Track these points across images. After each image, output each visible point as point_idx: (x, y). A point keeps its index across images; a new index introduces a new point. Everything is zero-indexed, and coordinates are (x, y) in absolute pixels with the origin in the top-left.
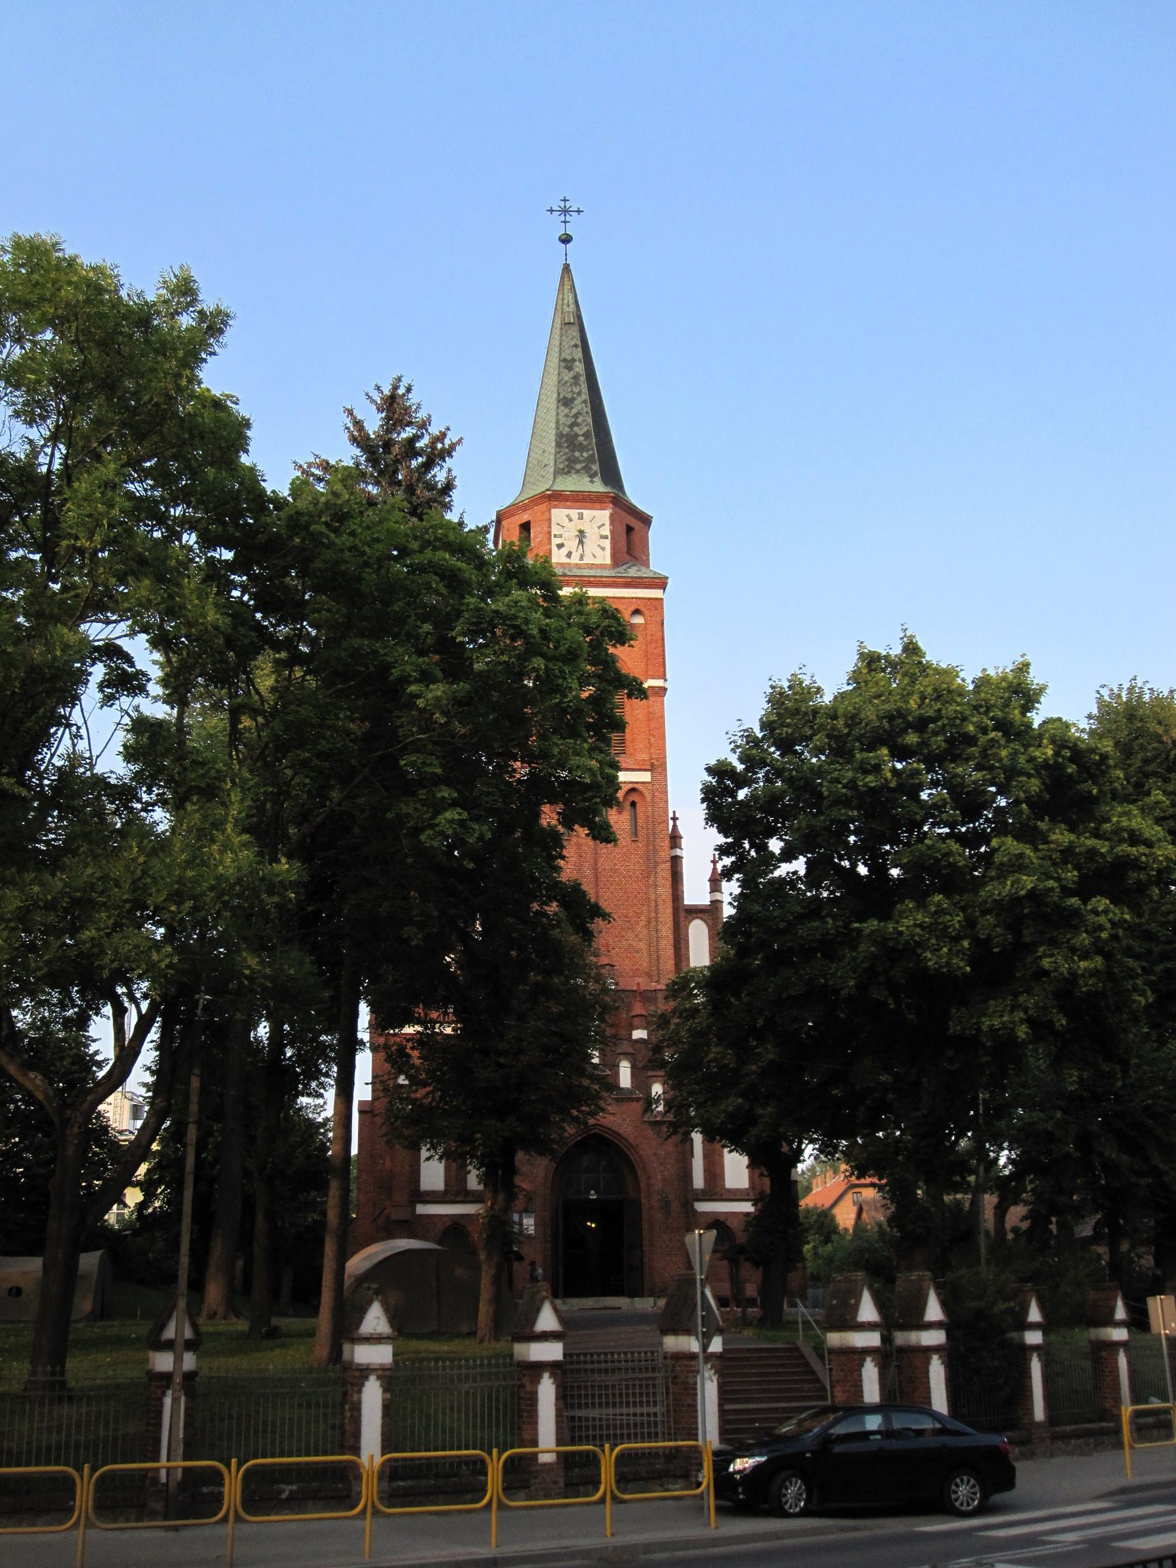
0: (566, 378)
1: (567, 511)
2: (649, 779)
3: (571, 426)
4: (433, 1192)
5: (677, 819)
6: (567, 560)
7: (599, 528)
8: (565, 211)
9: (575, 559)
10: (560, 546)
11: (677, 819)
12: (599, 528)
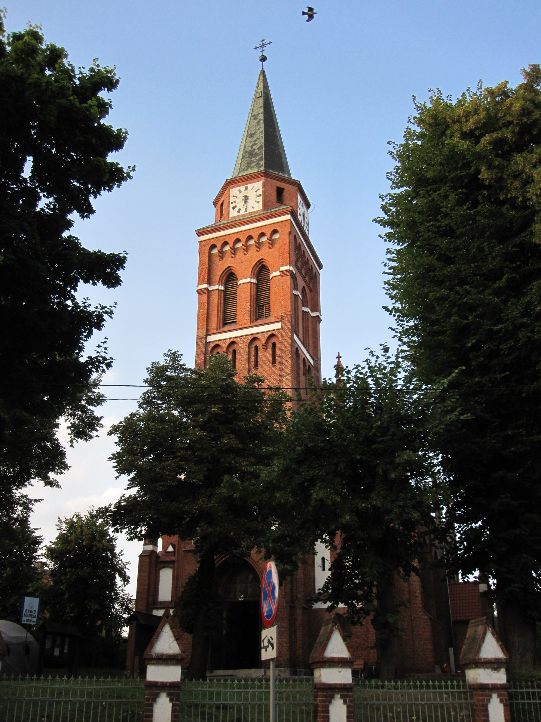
0: (253, 124)
1: (238, 188)
2: (280, 327)
3: (252, 147)
4: (165, 602)
5: (341, 357)
6: (238, 214)
7: (256, 192)
8: (263, 46)
9: (242, 212)
10: (234, 208)
11: (341, 357)
12: (256, 192)
